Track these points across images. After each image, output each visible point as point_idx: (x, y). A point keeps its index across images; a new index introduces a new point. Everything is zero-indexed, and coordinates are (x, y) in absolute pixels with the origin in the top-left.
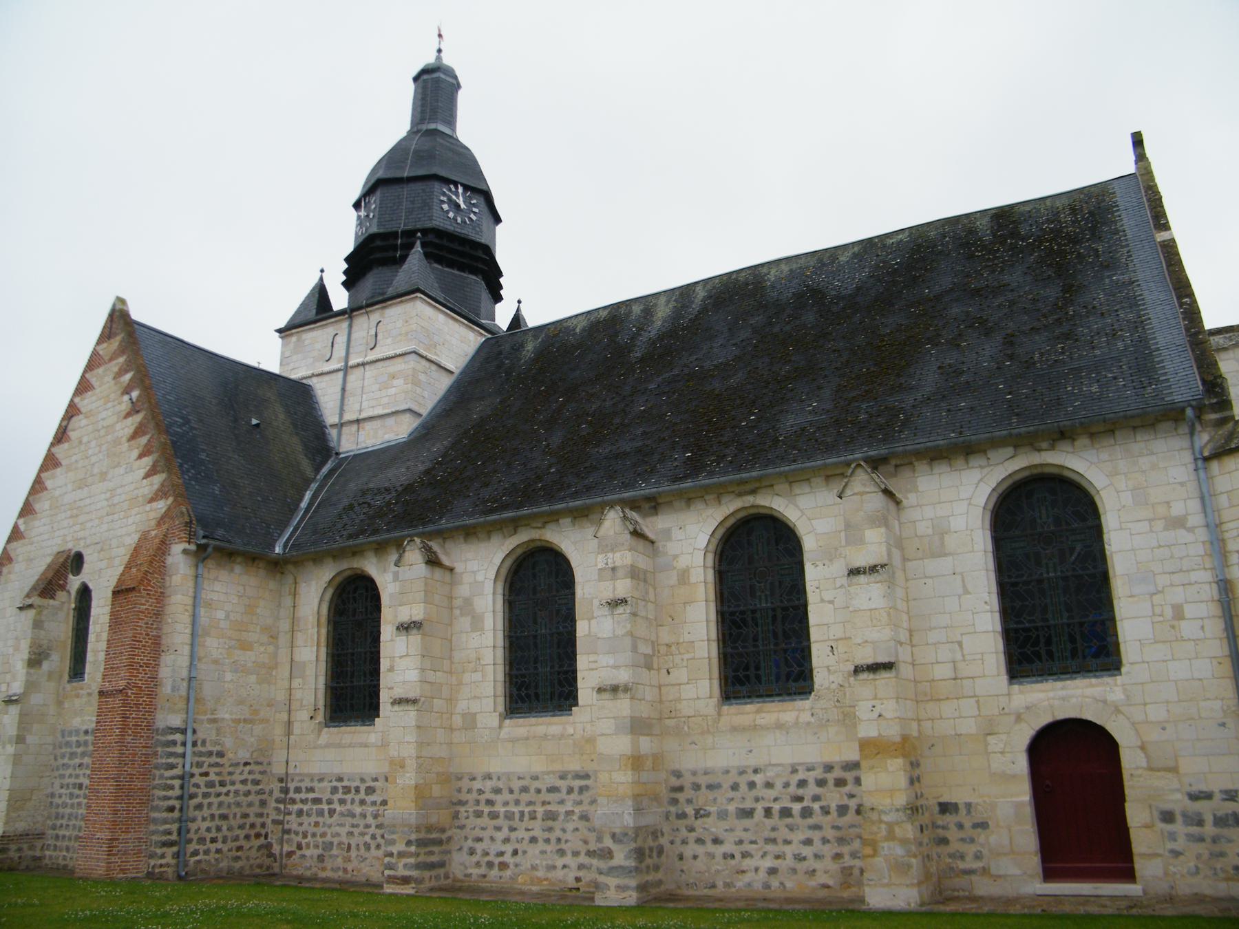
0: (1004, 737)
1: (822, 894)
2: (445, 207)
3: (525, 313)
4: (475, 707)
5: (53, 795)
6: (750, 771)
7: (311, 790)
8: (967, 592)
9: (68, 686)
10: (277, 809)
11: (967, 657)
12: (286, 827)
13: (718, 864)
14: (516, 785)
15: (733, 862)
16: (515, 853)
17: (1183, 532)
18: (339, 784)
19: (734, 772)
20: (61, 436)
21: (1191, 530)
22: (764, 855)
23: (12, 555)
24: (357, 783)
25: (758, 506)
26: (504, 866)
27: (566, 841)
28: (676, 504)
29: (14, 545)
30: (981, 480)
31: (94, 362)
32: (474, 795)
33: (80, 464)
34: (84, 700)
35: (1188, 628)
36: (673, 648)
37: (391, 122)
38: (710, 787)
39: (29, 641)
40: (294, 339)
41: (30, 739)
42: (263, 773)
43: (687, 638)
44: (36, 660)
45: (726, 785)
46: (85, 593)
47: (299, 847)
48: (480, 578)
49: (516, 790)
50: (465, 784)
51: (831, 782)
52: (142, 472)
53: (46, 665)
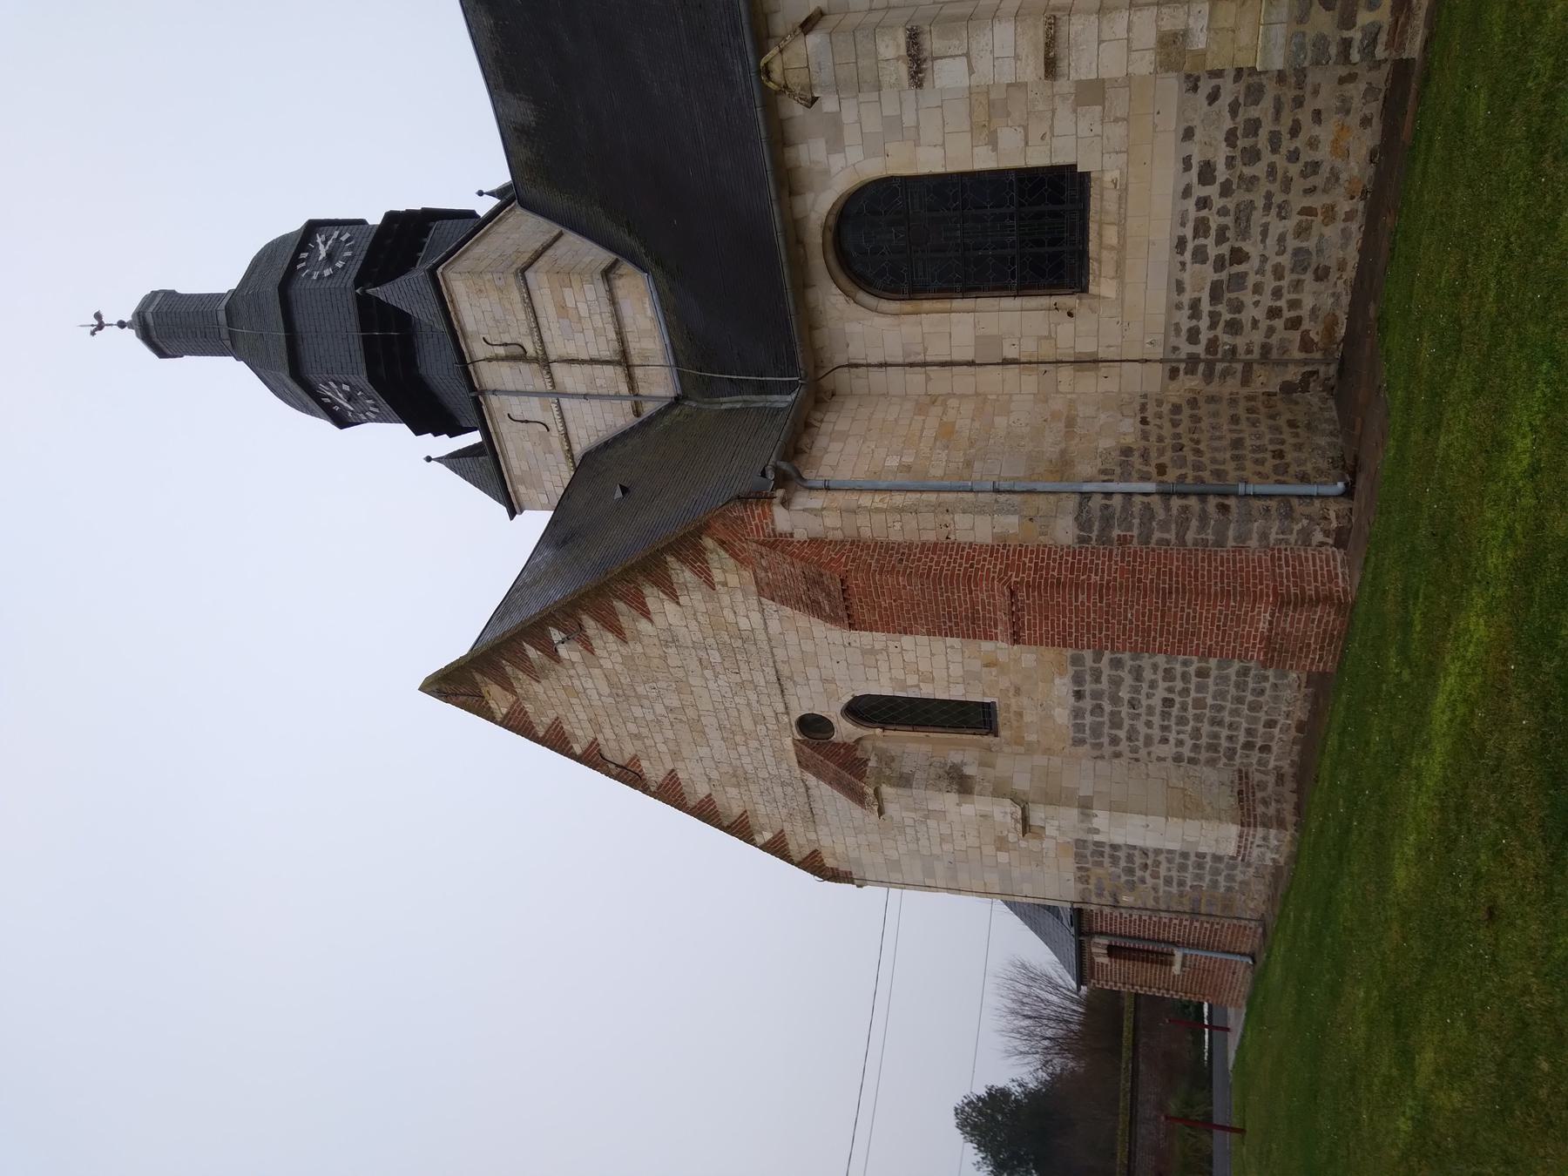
2: (327, 272)
3: (495, 186)
5: (1178, 759)
7: (1195, 305)
9: (1004, 733)
10: (1225, 374)
12: (1256, 355)
18: (1190, 247)
20: (630, 775)
23: (807, 852)
24: (1190, 204)
29: (792, 847)
31: (518, 723)
33: (670, 734)
34: (1025, 701)
37: (226, 384)
39: (930, 793)
40: (522, 489)
41: (1085, 791)
42: (1160, 403)
44: (962, 784)
46: (864, 710)
47: (1294, 323)
52: (670, 607)
53: (969, 770)
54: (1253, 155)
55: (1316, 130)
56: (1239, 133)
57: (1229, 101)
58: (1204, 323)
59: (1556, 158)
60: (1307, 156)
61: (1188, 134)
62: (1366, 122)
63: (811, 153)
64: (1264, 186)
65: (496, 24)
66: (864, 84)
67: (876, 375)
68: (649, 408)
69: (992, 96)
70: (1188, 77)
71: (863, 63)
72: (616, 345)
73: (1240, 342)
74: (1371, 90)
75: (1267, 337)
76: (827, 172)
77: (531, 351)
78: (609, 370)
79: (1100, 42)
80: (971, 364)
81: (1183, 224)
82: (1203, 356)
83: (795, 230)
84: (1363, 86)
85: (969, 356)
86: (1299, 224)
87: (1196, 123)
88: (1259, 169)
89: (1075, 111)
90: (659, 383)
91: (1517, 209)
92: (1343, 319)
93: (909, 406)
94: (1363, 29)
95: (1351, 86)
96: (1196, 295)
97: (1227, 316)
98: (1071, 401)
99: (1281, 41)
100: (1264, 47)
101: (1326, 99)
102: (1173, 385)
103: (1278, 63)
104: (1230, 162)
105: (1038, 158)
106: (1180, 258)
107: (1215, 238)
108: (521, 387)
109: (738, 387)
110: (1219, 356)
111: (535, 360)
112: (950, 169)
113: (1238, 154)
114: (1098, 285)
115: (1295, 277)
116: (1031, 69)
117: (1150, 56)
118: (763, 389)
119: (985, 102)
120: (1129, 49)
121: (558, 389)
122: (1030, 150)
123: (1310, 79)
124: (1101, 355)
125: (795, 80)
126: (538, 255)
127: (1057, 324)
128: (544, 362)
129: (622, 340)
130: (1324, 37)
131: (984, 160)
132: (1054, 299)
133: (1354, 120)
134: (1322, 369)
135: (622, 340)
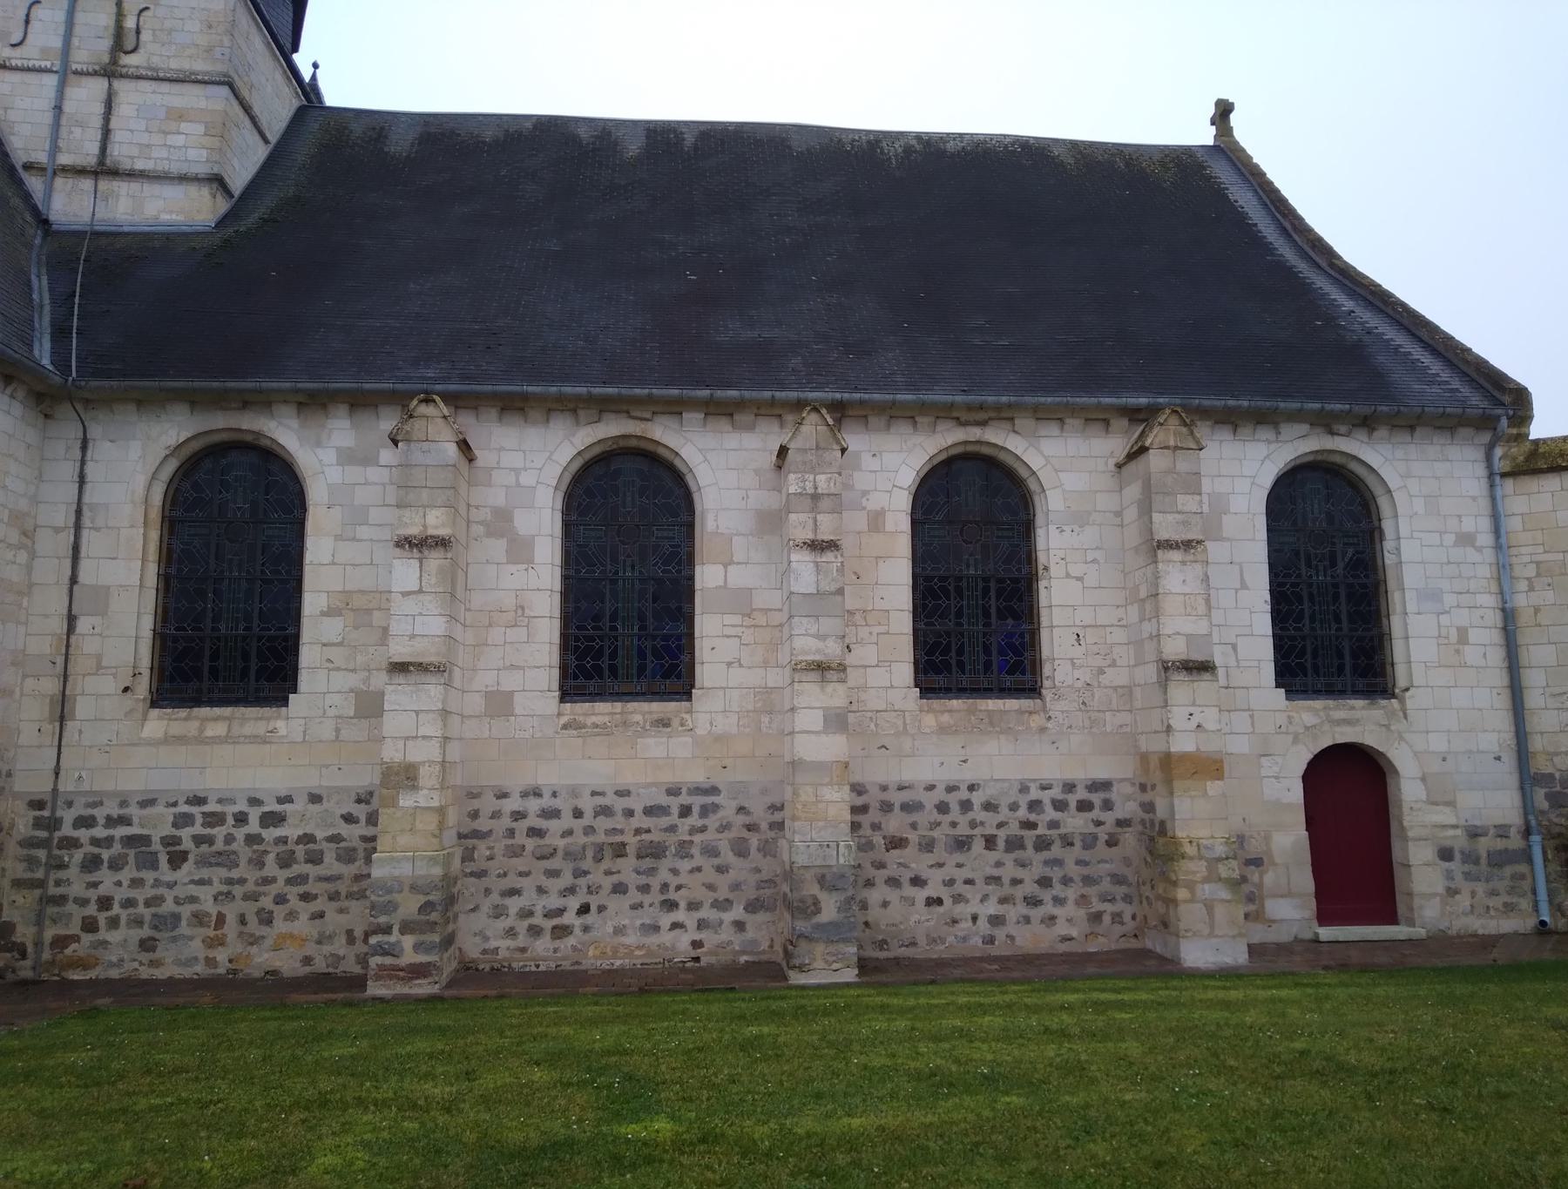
0: (1279, 759)
1: (1063, 948)
4: (510, 682)
6: (964, 787)
7: (124, 821)
8: (1244, 586)
10: (31, 862)
11: (1243, 664)
12: (53, 890)
13: (920, 913)
14: (587, 804)
15: (941, 909)
16: (584, 909)
17: (1470, 550)
19: (941, 788)
21: (1479, 550)
22: (984, 898)
25: (989, 444)
26: (561, 932)
27: (679, 888)
28: (873, 420)
30: (1267, 457)
32: (506, 822)
35: (1471, 654)
36: (858, 617)
38: (906, 807)
43: (879, 605)
45: (929, 806)
48: (527, 479)
49: (589, 814)
50: (488, 804)
51: (1073, 805)
54: (285, 861)
55: (304, 917)
56: (311, 846)
57: (344, 833)
58: (100, 832)
59: (304, 1121)
60: (279, 912)
61: (315, 798)
62: (307, 960)
63: (341, 431)
64: (252, 875)
65: (484, 143)
66: (405, 492)
67: (69, 470)
68: (35, 184)
69: (376, 614)
70: (371, 794)
71: (425, 494)
72: (126, 165)
73: (73, 872)
74: (338, 959)
75: (76, 900)
76: (318, 444)
77: (127, 60)
78: (94, 148)
79: (417, 713)
80: (74, 580)
81: (220, 801)
82: (57, 834)
83: (263, 402)
84: (341, 952)
85: (83, 577)
86: (208, 914)
87: (325, 804)
88: (271, 868)
89: (352, 691)
90: (70, 205)
91: (250, 1102)
92: (92, 974)
93: (23, 505)
94: (399, 942)
95: (344, 941)
96: (135, 820)
97: (106, 855)
98: (12, 693)
99: (396, 873)
100: (392, 858)
101: (334, 921)
102: (21, 806)
103: (377, 872)
104: (283, 840)
105: (308, 655)
106: (182, 800)
107: (203, 833)
108: (77, 30)
109: (62, 301)
110: (56, 852)
111: (114, 61)
112: (307, 570)
113: (289, 847)
114: (160, 718)
115: (148, 918)
116: (400, 650)
117: (398, 757)
118: (60, 333)
119: (371, 606)
120: (407, 738)
121: (72, 77)
122: (318, 648)
123: (354, 905)
124: (69, 725)
125: (417, 426)
126: (247, 109)
127: (115, 676)
128: (110, 72)
129: (132, 175)
130: (395, 909)
131: (312, 603)
132: (146, 673)
133: (311, 949)
134: (28, 963)
135: (132, 175)
